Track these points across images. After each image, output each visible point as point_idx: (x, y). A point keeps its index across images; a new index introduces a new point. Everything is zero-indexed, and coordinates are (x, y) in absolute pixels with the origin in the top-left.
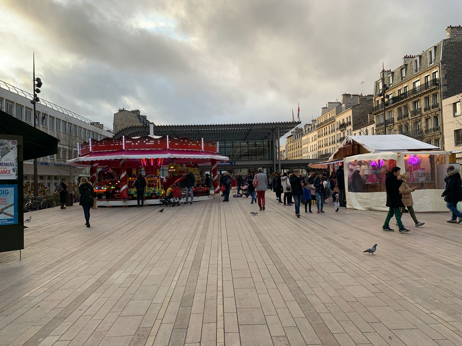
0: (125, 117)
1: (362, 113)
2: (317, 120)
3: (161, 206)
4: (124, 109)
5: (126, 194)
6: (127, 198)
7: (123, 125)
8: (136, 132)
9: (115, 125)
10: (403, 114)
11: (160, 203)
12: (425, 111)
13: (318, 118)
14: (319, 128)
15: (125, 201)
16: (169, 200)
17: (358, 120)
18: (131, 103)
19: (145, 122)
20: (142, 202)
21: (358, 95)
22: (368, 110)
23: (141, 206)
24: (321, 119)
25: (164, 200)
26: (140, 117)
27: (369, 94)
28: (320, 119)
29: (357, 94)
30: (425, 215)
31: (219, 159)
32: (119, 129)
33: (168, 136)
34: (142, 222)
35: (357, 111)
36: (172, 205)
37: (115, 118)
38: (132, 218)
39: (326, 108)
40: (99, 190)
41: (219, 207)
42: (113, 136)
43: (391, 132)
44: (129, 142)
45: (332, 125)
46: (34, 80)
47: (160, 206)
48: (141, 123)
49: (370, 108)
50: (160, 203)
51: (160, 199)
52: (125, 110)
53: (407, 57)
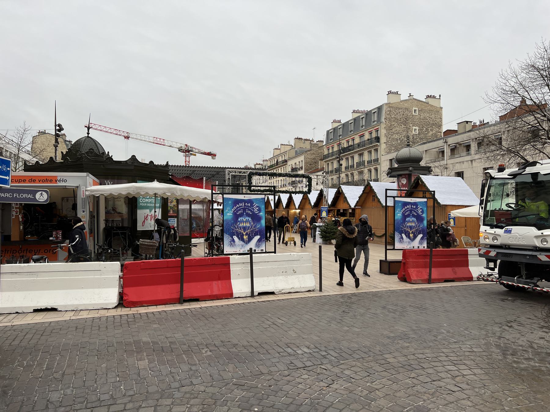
0: (47, 141)
1: (314, 159)
10: (350, 165)
13: (270, 159)
21: (309, 140)
24: (273, 160)
27: (320, 140)
29: (308, 139)
31: (116, 193)
33: (204, 178)
39: (278, 149)
41: (410, 153)
45: (284, 168)
46: (56, 126)
53: (355, 112)
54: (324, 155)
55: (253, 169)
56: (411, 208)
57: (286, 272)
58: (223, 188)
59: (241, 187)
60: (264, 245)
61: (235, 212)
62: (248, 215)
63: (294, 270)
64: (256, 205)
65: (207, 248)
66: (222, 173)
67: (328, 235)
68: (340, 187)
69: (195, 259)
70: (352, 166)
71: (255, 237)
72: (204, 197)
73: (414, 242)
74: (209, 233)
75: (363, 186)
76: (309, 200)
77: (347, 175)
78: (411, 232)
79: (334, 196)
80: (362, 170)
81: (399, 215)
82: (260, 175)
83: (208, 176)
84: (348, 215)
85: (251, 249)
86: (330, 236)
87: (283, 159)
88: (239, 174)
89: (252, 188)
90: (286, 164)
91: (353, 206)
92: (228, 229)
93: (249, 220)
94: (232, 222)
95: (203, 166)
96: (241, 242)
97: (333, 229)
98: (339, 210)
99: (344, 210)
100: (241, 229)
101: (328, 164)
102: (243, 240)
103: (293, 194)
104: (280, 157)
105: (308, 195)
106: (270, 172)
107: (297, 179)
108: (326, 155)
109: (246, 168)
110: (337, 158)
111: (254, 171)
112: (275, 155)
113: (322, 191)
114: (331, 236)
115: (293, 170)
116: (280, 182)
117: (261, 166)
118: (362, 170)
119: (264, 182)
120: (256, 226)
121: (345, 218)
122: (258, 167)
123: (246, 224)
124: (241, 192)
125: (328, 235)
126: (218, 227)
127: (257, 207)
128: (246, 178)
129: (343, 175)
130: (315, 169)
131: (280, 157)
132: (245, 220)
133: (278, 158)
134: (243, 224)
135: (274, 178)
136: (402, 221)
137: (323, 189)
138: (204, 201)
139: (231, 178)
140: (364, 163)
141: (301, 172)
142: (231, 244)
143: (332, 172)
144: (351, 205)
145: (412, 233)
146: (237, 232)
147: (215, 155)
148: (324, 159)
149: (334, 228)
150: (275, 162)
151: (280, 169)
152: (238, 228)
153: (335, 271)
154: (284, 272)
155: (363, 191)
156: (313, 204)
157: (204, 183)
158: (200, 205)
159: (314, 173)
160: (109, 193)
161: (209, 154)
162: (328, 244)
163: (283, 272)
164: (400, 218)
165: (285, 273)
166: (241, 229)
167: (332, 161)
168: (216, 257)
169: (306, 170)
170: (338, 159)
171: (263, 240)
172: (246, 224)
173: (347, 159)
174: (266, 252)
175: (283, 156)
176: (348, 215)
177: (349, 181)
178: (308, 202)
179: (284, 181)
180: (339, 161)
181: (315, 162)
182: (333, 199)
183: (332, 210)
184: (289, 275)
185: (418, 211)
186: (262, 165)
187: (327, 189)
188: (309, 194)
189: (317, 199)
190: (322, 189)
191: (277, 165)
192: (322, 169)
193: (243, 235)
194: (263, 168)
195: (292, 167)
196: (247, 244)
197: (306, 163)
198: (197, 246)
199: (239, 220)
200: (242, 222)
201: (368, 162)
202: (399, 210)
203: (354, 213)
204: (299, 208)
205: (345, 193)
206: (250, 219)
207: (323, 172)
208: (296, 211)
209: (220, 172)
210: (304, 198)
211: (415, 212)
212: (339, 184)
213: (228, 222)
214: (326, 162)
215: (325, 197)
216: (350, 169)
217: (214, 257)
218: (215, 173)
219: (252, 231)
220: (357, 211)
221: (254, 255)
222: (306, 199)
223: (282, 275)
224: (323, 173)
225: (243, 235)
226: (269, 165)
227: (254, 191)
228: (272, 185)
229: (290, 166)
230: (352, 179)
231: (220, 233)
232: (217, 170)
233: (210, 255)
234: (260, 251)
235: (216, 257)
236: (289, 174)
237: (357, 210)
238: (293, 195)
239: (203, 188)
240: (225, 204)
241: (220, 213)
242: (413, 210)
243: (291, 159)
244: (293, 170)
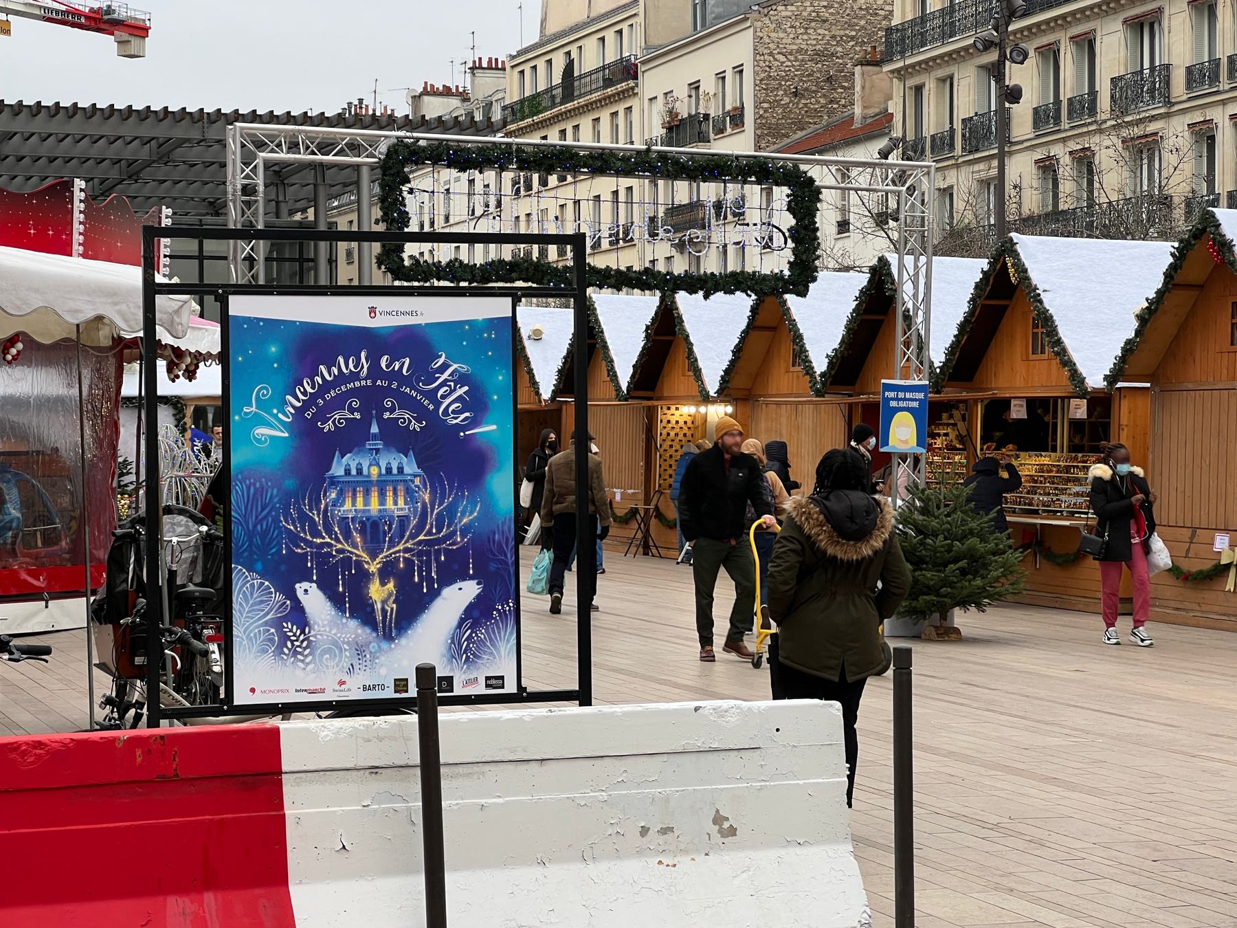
1: (819, 55)
2: (508, 67)
10: (1067, 92)
12: (1189, 85)
13: (520, 53)
14: (522, 124)
17: (786, 100)
22: (852, 38)
24: (541, 64)
28: (532, 64)
30: (1048, 616)
33: (79, 184)
35: (781, 35)
40: (374, 382)
43: (1145, 167)
44: (471, 566)
45: (615, 114)
49: (863, 22)
54: (889, 31)
55: (407, 123)
56: (375, 372)
57: (665, 831)
58: (201, 257)
59: (323, 246)
60: (506, 647)
61: (308, 415)
62: (396, 438)
63: (718, 819)
64: (448, 365)
65: (103, 666)
66: (194, 154)
67: (929, 575)
68: (1009, 248)
69: (39, 744)
70: (1085, 106)
71: (446, 592)
72: (89, 314)
73: (403, 641)
74: (116, 563)
75: (1163, 236)
76: (798, 338)
77: (1047, 168)
78: (373, 568)
79: (965, 308)
80: (1152, 127)
81: (262, 431)
82: (463, 160)
83: (99, 173)
84: (1063, 436)
85: (425, 673)
86: (945, 583)
87: (611, 57)
88: (319, 157)
89: (411, 249)
90: (630, 93)
91: (1095, 379)
92: (264, 534)
93: (401, 470)
94: (290, 484)
95: (139, 106)
96: (353, 623)
97: (963, 538)
98: (998, 408)
99: (1032, 403)
100: (348, 536)
101: (919, 89)
102: (361, 609)
103: (692, 290)
104: (591, 45)
105: (791, 299)
106: (535, 139)
107: (709, 191)
108: (902, 29)
109: (353, 117)
110: (988, 45)
111: (424, 138)
112: (552, 29)
113: (880, 275)
114: (951, 585)
115: (677, 128)
116: (606, 208)
117: (455, 102)
118: (1152, 127)
119: (492, 209)
120: (451, 511)
121: (765, 461)
122: (434, 108)
123: (382, 502)
124: (323, 281)
125: (929, 575)
126: (181, 519)
127: (461, 379)
128: (357, 183)
129: (1021, 168)
130: (829, 129)
131: (591, 45)
132: (374, 471)
133: (573, 49)
134: (360, 500)
135: (544, 183)
136: (290, 484)
137: (893, 258)
138: (84, 340)
139: (266, 186)
140: (1167, 83)
141: (738, 145)
142: (284, 638)
143: (942, 144)
144: (1082, 369)
145: (384, 574)
146: (322, 557)
147: (140, 31)
148: (887, 58)
149: (973, 525)
150: (557, 79)
151: (586, 123)
152: (329, 531)
153: (994, 819)
154: (655, 828)
155: (1169, 275)
156: (820, 365)
157: (78, 217)
158: (53, 372)
159: (820, 153)
160: (37, 302)
161: (99, 21)
162: (929, 640)
163: (644, 831)
164: (276, 458)
165: (661, 839)
166: (348, 536)
167: (941, 73)
168: (179, 728)
169: (766, 131)
170: (993, 56)
171: (503, 614)
172: (382, 502)
173: (1051, 54)
174: (522, 696)
175: (610, 35)
176: (1063, 436)
177: (1062, 207)
178: (787, 350)
179: (616, 200)
180: (996, 71)
181: (829, 79)
182: (962, 327)
183: (948, 406)
184: (685, 852)
185: (431, 395)
186: (464, 97)
187: (923, 259)
188: (803, 293)
189: (849, 328)
190: (883, 262)
191: (568, 93)
192: (879, 125)
193: (365, 576)
194: (470, 115)
195: (672, 113)
196: (389, 637)
197: (765, 85)
198: (47, 651)
199: (337, 470)
200: (358, 484)
201: (1194, 76)
202: (262, 390)
203: (1106, 427)
204: (726, 391)
205: (1041, 287)
206: (411, 467)
207: (883, 143)
208: (702, 409)
209: (181, 142)
210: (760, 320)
211: (406, 403)
212: (1003, 226)
213: (261, 491)
214: (900, 74)
215: (907, 318)
216: (1065, 124)
217: (166, 728)
218: (144, 153)
219: (426, 552)
220: (1125, 414)
221: (445, 715)
222: (774, 329)
223: (640, 853)
224: (884, 154)
225: (365, 576)
226: (513, 96)
227: (422, 270)
228: (570, 230)
229: (660, 105)
230: (1080, 188)
231: (194, 561)
232: (162, 131)
233: (138, 717)
234: (481, 689)
235: (179, 728)
236: (663, 156)
237: (1125, 405)
238: (682, 298)
239: (69, 254)
240: (237, 359)
241: (183, 431)
242: (387, 392)
243: (660, 54)
244: (677, 128)
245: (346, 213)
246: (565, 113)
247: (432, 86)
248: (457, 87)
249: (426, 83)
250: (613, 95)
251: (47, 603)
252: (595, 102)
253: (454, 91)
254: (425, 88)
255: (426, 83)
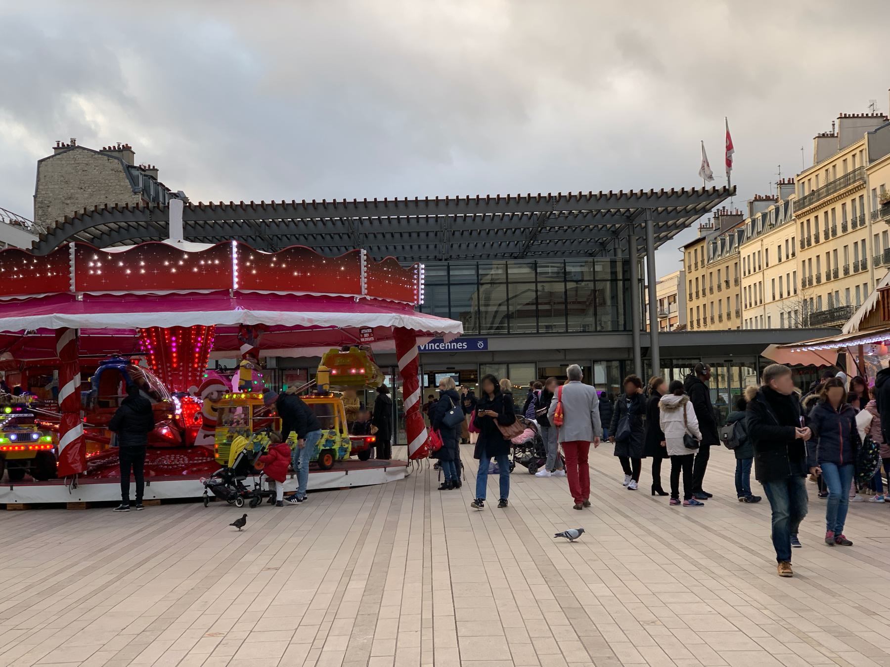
2: (795, 182)
3: (209, 504)
4: (73, 141)
5: (78, 458)
6: (81, 476)
7: (68, 202)
8: (120, 227)
9: (42, 202)
11: (206, 492)
15: (75, 486)
16: (239, 481)
18: (101, 119)
19: (152, 193)
20: (140, 491)
23: (133, 504)
25: (220, 484)
26: (135, 173)
28: (808, 178)
32: (57, 215)
33: (235, 243)
34: (140, 564)
36: (247, 501)
37: (42, 176)
38: (101, 550)
42: (33, 242)
45: (853, 201)
47: (206, 507)
48: (135, 193)
50: (206, 492)
51: (204, 479)
52: (79, 147)
245: (717, 266)
246: (827, 202)
247: (63, 144)
248: (773, 196)
249: (756, 195)
250: (852, 190)
251: (385, 469)
252: (843, 194)
253: (771, 198)
254: (756, 198)
255: (756, 195)
